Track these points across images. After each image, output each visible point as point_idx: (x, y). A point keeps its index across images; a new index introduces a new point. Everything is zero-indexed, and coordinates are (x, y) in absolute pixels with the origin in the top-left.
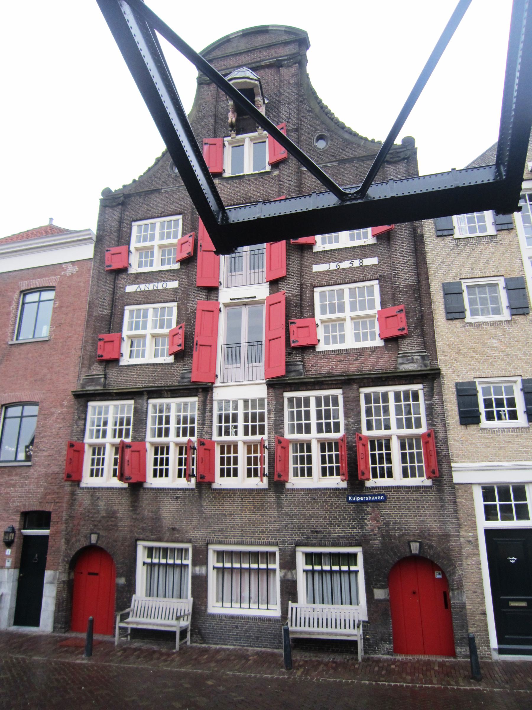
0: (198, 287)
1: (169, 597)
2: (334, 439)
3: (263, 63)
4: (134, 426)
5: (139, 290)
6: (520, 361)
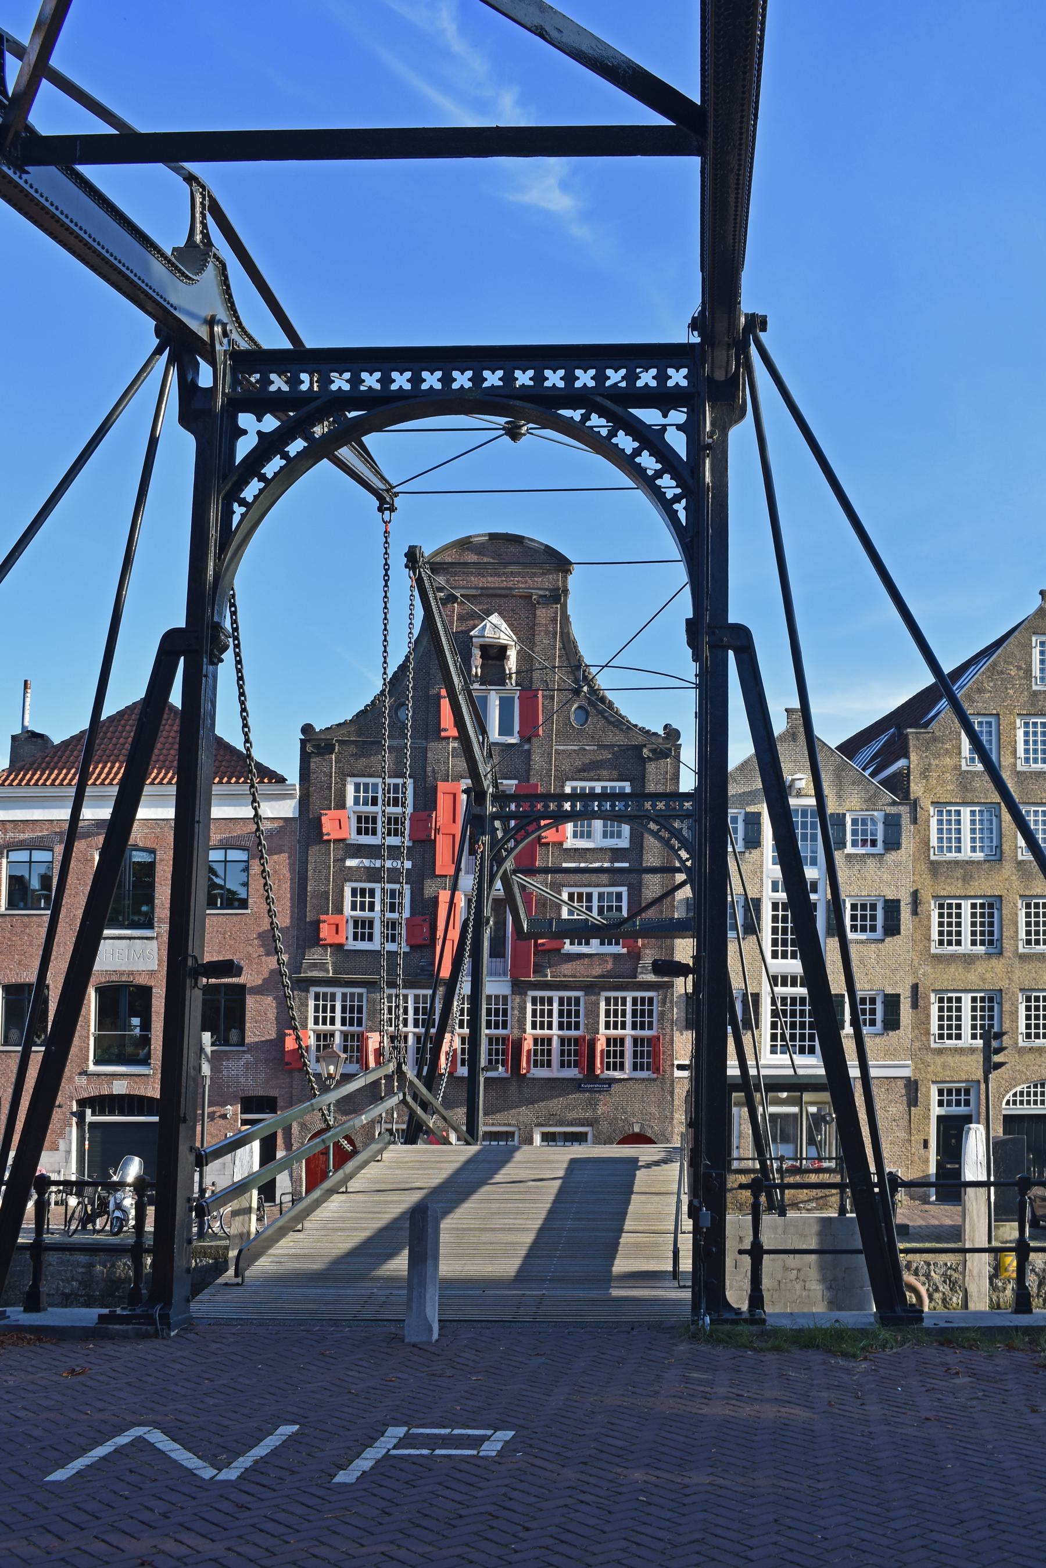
2: (501, 1035)
3: (515, 592)
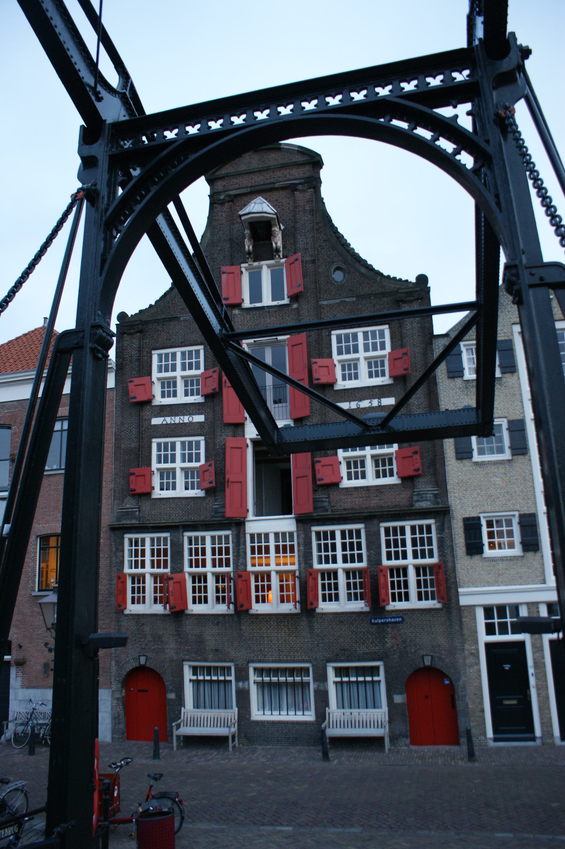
0: (225, 424)
1: (215, 708)
3: (277, 185)
4: (171, 557)
5: (165, 423)
6: (518, 497)
